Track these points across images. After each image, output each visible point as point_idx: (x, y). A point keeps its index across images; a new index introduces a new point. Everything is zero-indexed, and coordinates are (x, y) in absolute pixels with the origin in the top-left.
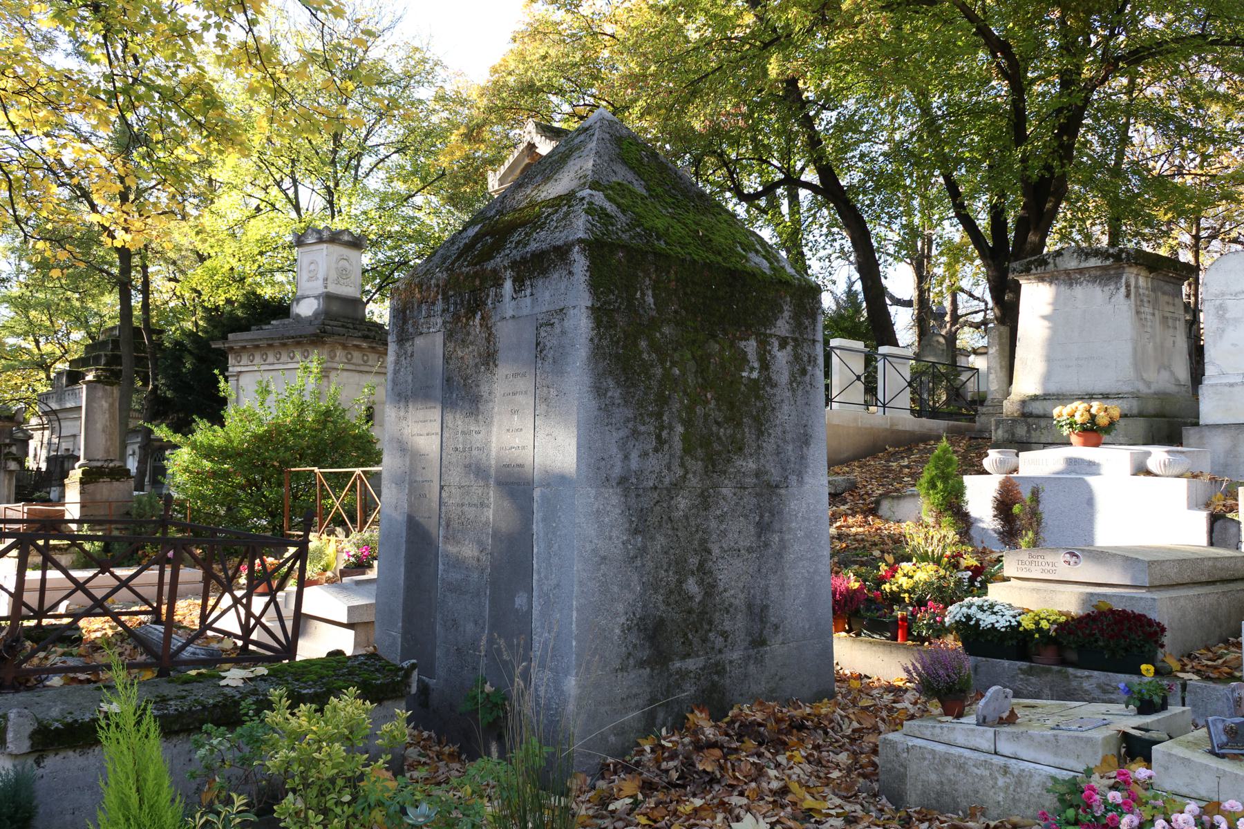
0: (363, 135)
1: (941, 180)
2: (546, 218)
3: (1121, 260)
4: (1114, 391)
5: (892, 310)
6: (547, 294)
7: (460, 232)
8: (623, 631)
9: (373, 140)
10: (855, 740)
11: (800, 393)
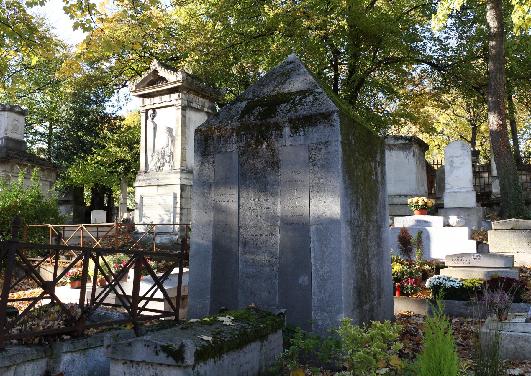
3: (412, 141)
4: (409, 194)
6: (316, 135)
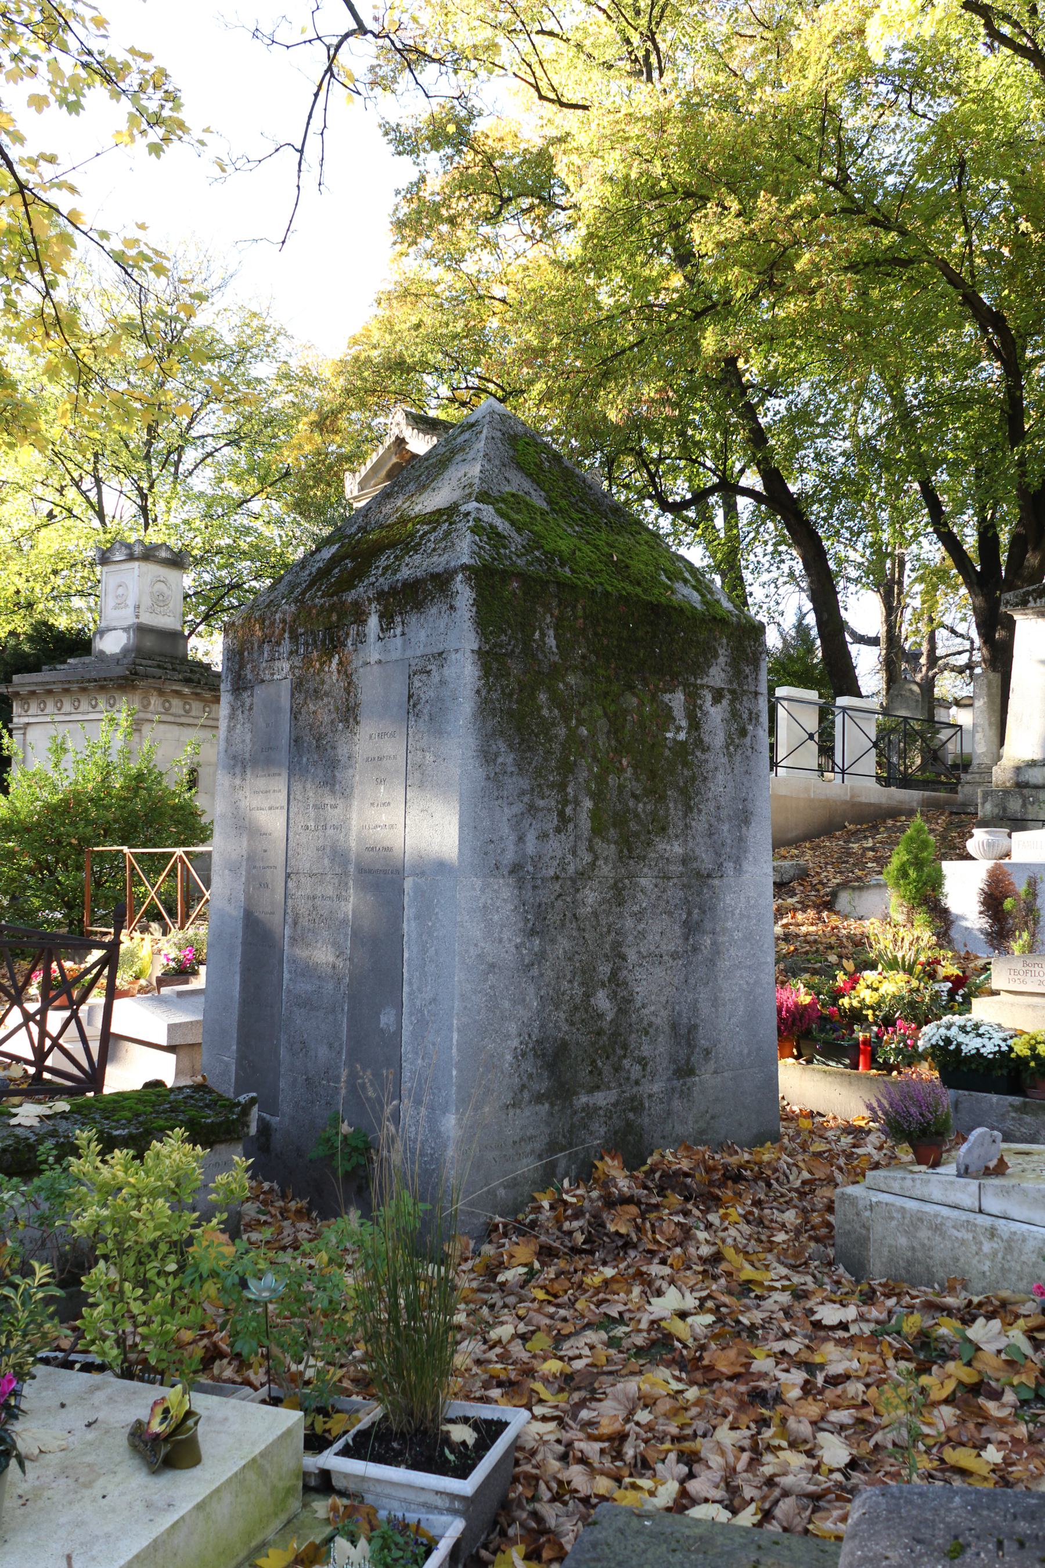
0: (185, 423)
1: (916, 486)
2: (422, 537)
5: (854, 649)
6: (423, 634)
7: (313, 554)
8: (516, 1057)
9: (198, 430)
10: (805, 1194)
11: (738, 758)
